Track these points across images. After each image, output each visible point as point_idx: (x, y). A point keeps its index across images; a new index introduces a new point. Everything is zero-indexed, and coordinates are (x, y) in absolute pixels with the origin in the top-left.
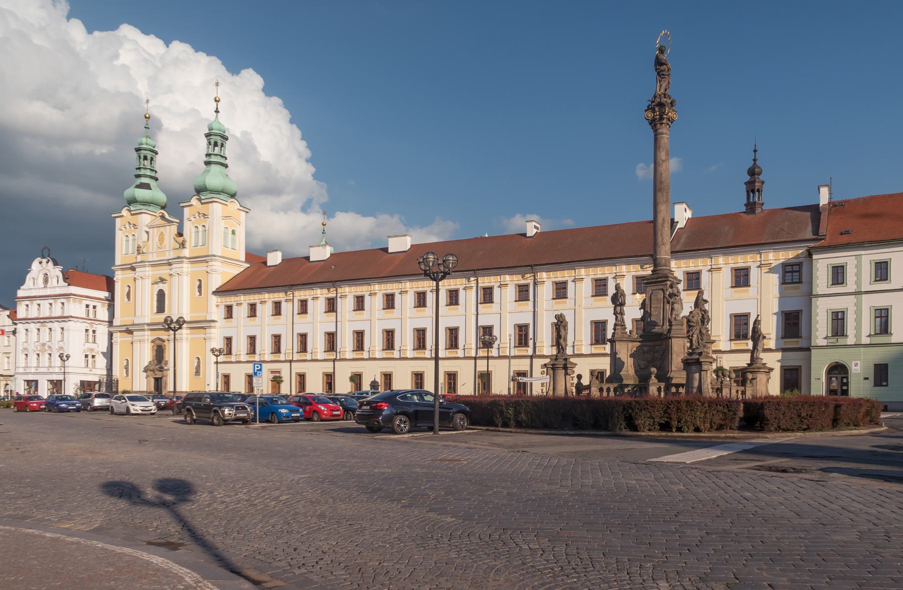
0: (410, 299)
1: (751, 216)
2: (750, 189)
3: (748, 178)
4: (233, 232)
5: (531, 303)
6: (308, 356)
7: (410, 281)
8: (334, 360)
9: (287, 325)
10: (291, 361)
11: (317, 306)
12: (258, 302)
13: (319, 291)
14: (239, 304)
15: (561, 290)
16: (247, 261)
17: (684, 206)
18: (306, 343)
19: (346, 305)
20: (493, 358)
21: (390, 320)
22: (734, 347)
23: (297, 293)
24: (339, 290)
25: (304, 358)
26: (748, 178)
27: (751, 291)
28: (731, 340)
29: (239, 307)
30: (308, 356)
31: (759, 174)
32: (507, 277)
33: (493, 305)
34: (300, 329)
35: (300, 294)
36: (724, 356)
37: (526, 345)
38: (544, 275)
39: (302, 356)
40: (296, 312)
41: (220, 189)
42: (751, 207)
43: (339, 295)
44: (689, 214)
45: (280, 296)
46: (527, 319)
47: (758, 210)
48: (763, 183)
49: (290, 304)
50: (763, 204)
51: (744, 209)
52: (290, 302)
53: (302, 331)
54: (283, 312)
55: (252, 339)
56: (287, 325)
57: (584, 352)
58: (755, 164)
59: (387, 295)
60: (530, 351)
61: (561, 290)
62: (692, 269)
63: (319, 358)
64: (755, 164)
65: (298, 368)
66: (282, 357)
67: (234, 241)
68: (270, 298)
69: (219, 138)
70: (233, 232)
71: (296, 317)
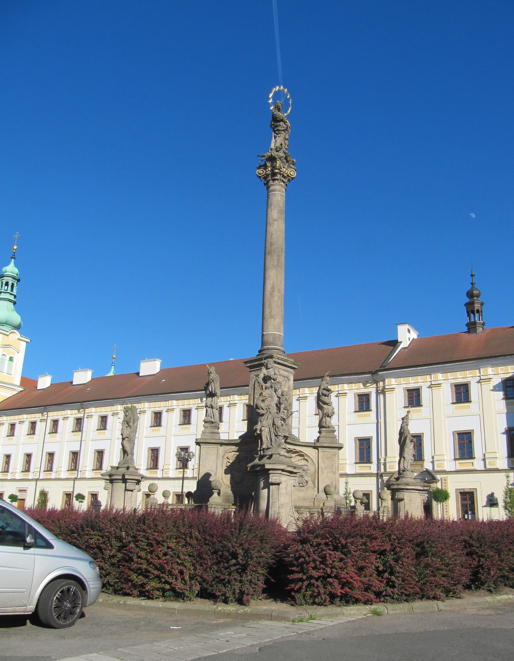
0: (176, 417)
1: (472, 336)
2: (470, 310)
3: (467, 300)
4: (11, 359)
5: (373, 414)
6: (53, 475)
7: (493, 366)
8: (75, 479)
9: (37, 446)
10: (37, 480)
11: (67, 426)
12: (17, 422)
13: (69, 412)
14: (21, 422)
15: (414, 398)
16: (22, 384)
17: (407, 327)
18: (102, 459)
19: (91, 424)
20: (188, 478)
21: (465, 418)
22: (459, 468)
23: (50, 414)
24: (87, 410)
25: (471, 468)
26: (467, 300)
27: (473, 407)
28: (455, 459)
29: (116, 417)
30: (53, 475)
31: (478, 296)
32: (440, 376)
33: (57, 435)
34: (49, 449)
35: (53, 415)
36: (450, 477)
37: (369, 461)
38: (393, 381)
39: (466, 464)
40: (48, 431)
41: (4, 321)
42: (472, 327)
43: (86, 415)
44: (414, 335)
45: (36, 417)
46: (369, 432)
47: (479, 330)
48: (482, 304)
49: (44, 423)
50: (483, 324)
51: (466, 329)
52: (43, 421)
53: (51, 450)
54: (37, 432)
55: (75, 455)
56: (37, 446)
57: (348, 472)
58: (473, 287)
59: (32, 423)
60: (373, 468)
61: (414, 398)
62: (412, 386)
63: (62, 477)
64: (473, 287)
65: (42, 486)
66: (30, 476)
67: (10, 367)
68: (27, 418)
69: (11, 278)
70: (11, 359)
71: (48, 436)
